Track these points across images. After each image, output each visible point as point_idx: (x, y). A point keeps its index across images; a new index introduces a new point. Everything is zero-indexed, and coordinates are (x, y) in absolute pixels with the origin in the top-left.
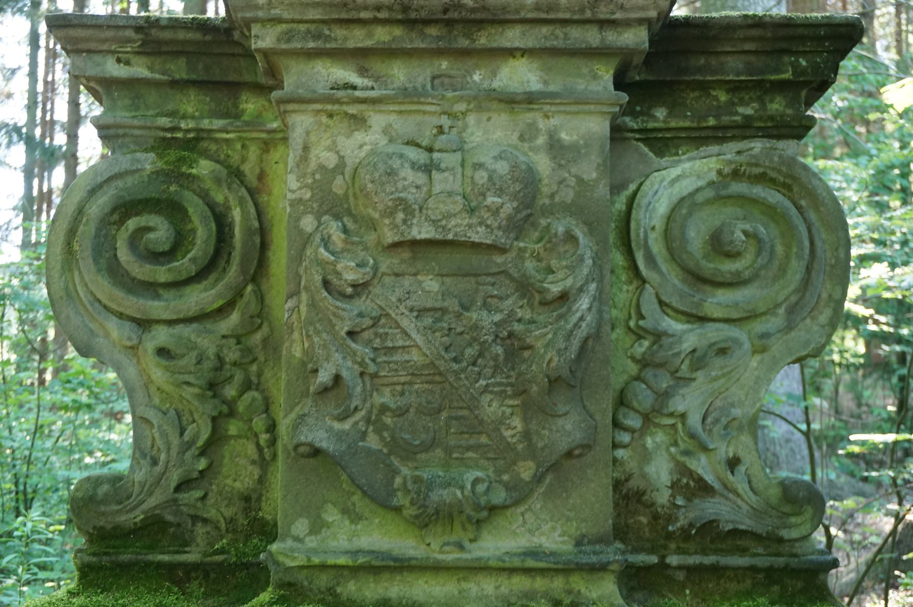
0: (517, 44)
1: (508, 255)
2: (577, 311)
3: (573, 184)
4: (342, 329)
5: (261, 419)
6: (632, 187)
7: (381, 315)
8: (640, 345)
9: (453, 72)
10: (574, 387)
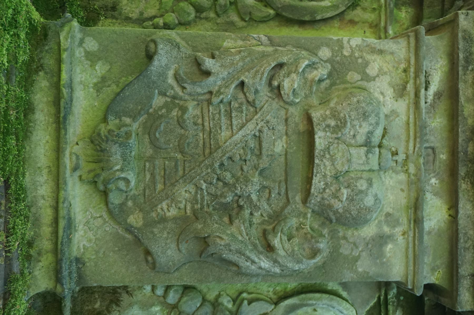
0: (461, 212)
1: (301, 205)
2: (259, 259)
3: (353, 254)
4: (245, 77)
5: (174, 19)
6: (344, 294)
7: (256, 108)
8: (229, 301)
9: (437, 163)
10: (200, 257)
